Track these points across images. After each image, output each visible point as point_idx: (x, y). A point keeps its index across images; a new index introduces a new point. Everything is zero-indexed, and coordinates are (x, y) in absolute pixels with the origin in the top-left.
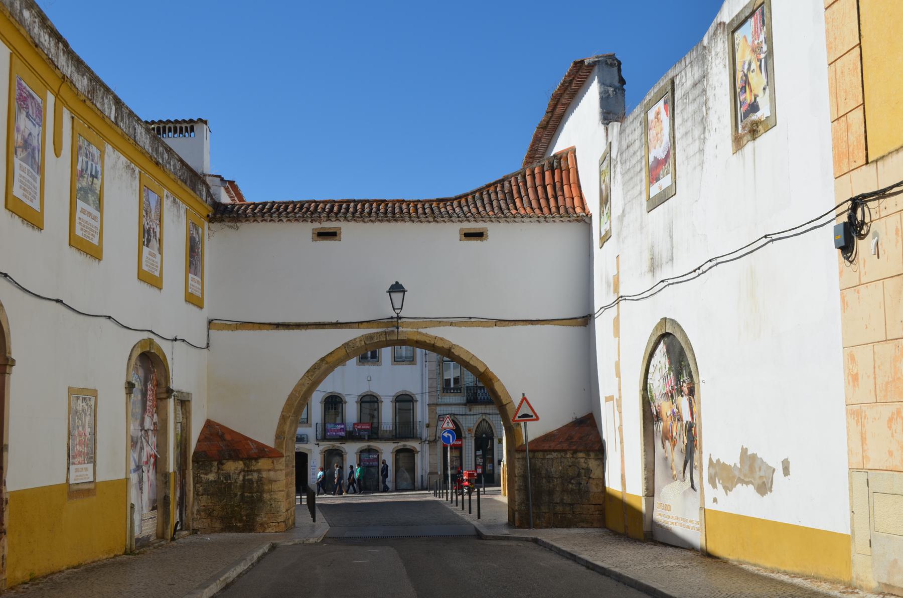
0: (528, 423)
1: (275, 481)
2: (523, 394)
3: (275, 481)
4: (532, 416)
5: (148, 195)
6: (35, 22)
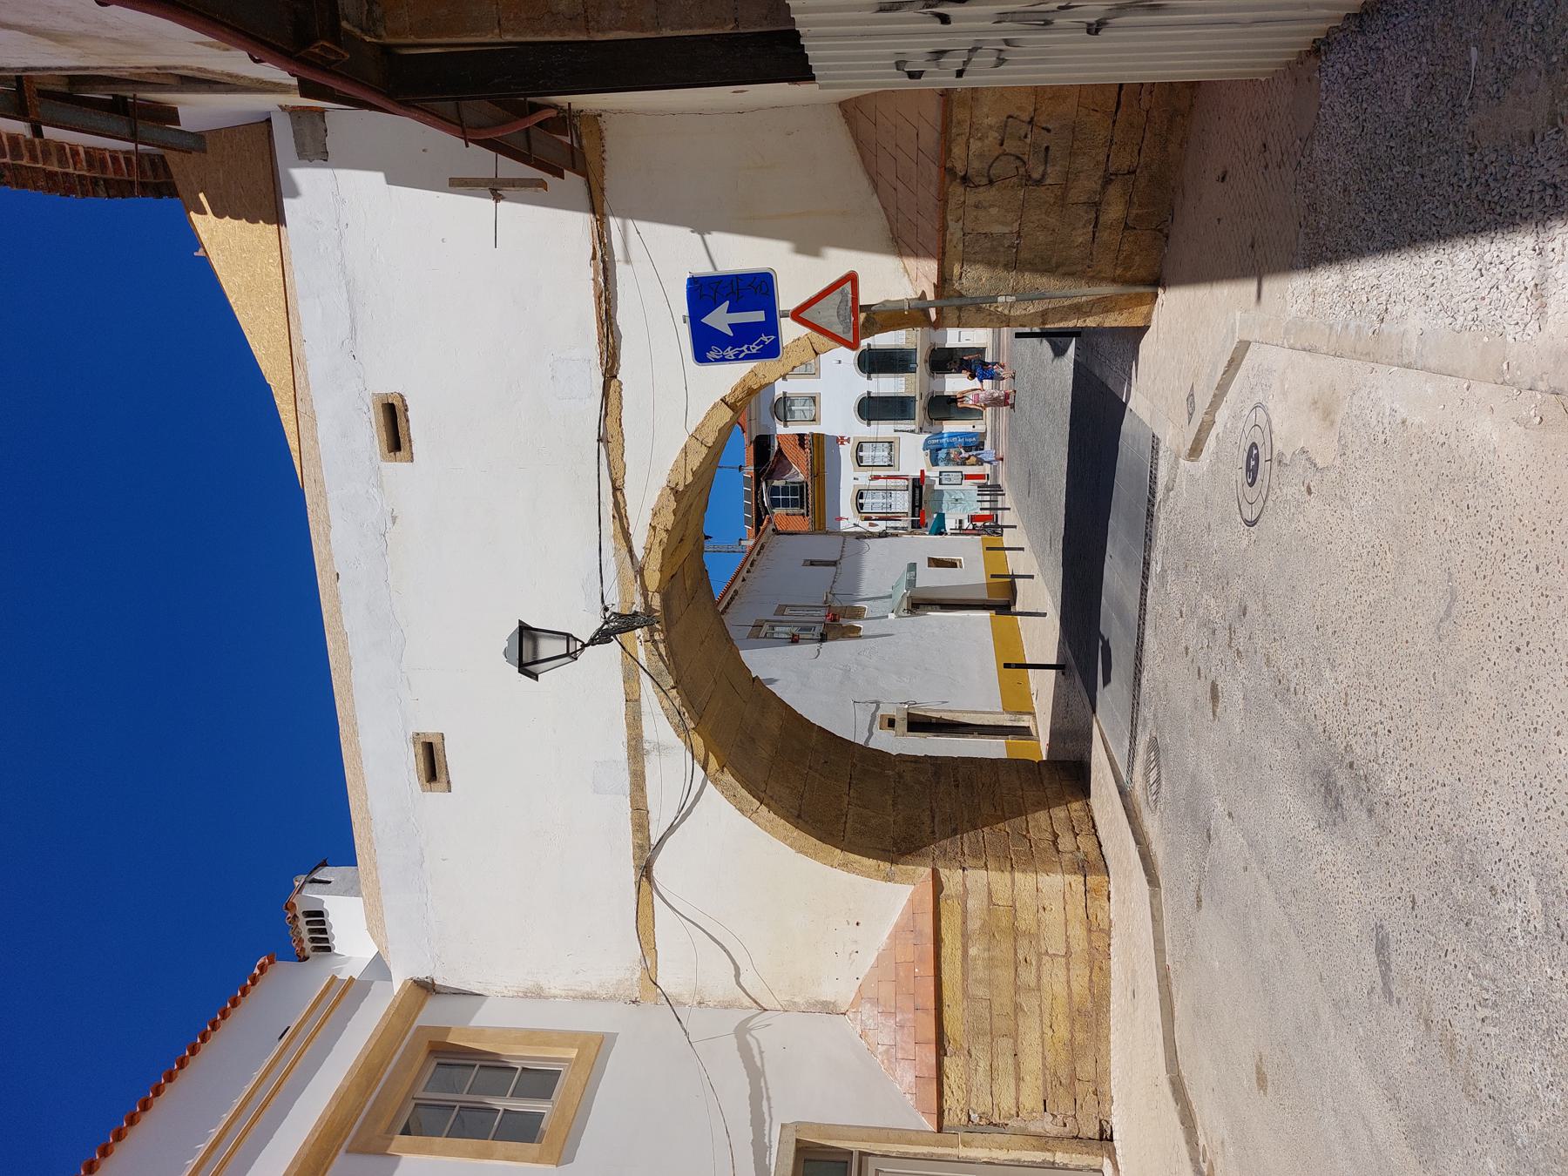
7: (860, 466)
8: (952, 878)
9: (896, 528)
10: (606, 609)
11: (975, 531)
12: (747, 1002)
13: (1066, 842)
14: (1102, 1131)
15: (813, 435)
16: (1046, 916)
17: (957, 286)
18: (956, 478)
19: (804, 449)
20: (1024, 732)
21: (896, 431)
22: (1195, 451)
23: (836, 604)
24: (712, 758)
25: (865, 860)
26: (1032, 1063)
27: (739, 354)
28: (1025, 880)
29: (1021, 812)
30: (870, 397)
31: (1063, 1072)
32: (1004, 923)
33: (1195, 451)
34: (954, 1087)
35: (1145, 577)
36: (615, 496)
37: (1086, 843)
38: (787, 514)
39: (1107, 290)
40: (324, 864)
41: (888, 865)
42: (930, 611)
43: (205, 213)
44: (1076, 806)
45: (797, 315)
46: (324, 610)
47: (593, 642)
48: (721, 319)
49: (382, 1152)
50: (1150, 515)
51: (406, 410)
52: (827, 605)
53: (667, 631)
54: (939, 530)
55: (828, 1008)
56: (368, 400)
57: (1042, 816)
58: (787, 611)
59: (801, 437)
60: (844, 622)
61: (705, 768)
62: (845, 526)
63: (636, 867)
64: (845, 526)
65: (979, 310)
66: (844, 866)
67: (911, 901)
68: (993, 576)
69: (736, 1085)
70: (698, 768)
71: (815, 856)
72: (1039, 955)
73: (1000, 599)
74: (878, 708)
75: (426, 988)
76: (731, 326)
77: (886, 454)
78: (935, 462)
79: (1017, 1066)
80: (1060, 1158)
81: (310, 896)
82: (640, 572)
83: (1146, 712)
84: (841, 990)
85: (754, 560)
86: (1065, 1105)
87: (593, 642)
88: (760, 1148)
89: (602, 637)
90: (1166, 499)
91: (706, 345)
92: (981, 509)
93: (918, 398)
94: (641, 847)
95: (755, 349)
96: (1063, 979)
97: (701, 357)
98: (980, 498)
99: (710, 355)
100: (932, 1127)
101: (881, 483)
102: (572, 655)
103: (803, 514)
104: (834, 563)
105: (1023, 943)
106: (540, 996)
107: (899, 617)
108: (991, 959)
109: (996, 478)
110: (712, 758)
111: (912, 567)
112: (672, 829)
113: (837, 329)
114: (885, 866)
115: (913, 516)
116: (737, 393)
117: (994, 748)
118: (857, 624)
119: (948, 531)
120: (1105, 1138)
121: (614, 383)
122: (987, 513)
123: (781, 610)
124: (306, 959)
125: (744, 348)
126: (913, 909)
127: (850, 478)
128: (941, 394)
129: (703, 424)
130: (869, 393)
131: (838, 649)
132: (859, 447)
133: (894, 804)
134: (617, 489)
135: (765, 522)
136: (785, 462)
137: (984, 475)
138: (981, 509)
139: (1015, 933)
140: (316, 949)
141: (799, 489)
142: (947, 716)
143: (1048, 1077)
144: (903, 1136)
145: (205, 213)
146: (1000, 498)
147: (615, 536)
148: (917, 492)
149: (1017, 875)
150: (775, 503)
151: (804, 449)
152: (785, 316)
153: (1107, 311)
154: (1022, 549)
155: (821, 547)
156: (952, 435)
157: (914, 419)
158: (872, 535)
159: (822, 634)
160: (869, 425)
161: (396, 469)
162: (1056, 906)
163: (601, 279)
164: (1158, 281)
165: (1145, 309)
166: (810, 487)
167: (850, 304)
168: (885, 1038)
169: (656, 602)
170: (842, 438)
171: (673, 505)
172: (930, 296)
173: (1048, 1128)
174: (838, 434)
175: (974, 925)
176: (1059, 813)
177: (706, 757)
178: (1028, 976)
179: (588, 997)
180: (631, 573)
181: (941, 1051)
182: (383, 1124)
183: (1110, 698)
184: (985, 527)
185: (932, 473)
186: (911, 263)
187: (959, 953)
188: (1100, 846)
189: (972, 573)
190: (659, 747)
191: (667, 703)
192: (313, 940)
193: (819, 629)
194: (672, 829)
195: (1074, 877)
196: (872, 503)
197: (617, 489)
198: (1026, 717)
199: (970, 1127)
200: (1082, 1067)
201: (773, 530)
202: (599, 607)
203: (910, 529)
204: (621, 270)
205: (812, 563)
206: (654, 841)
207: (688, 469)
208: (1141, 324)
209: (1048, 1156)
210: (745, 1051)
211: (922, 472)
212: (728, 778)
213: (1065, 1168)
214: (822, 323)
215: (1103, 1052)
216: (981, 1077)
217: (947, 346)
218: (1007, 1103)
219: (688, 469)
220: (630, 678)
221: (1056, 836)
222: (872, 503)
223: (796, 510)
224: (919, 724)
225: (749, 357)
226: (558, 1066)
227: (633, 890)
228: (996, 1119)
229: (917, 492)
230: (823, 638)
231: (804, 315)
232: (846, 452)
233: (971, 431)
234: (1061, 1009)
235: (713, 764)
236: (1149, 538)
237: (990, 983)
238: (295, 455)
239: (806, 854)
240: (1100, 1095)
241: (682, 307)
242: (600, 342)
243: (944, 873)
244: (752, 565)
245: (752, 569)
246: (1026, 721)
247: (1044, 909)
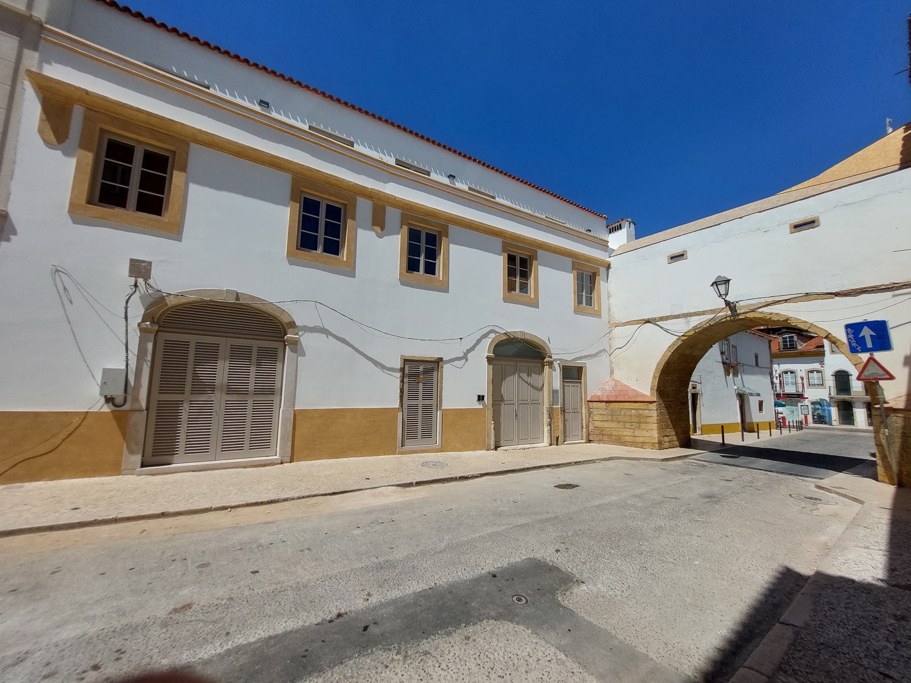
8: (654, 406)
9: (776, 387)
10: (737, 302)
11: (777, 419)
12: (612, 351)
13: (666, 439)
14: (591, 441)
15: (824, 351)
16: (645, 432)
17: (892, 415)
18: (805, 412)
19: (815, 348)
20: (695, 431)
21: (830, 387)
22: (819, 487)
23: (739, 367)
24: (686, 338)
26: (606, 425)
27: (850, 339)
28: (655, 426)
29: (674, 427)
30: (849, 375)
31: (604, 432)
32: (642, 420)
33: (819, 487)
35: (765, 470)
36: (783, 300)
37: (667, 445)
38: (779, 343)
39: (895, 467)
40: (635, 224)
41: (656, 389)
42: (739, 402)
43: (905, 132)
44: (677, 443)
45: (871, 359)
46: (726, 212)
47: (726, 301)
48: (867, 333)
49: (573, 269)
50: (791, 474)
51: (813, 228)
52: (738, 364)
53: (731, 321)
54: (776, 405)
55: (612, 372)
56: (816, 215)
57: (674, 433)
58: (734, 349)
59: (823, 346)
60: (731, 370)
61: (682, 336)
62: (775, 366)
63: (649, 319)
64: (775, 366)
65: (881, 422)
66: (654, 376)
67: (645, 395)
68: (758, 425)
69: (592, 351)
70: (682, 334)
72: (634, 429)
73: (747, 427)
74: (699, 383)
75: (608, 267)
76: (864, 336)
77: (816, 383)
78: (813, 403)
79: (605, 421)
80: (584, 430)
81: (626, 225)
82: (753, 311)
83: (715, 465)
84: (617, 375)
86: (596, 432)
87: (726, 301)
88: (580, 358)
89: (728, 304)
90: (798, 478)
91: (854, 329)
92: (789, 422)
93: (850, 396)
94: (655, 319)
95: (854, 345)
96: (628, 434)
97: (848, 326)
98: (795, 421)
99: (849, 330)
100: (588, 399)
101: (800, 381)
102: (720, 296)
103: (780, 349)
104: (757, 365)
105: (637, 425)
106: (608, 297)
107: (735, 390)
108: (632, 416)
109: (805, 428)
110: (686, 338)
111: (758, 395)
112: (662, 328)
113: (866, 373)
115: (783, 394)
118: (731, 375)
119: (776, 408)
120: (590, 441)
121: (833, 296)
122: (787, 424)
123: (734, 347)
124: (607, 227)
125: (854, 341)
126: (637, 394)
127: (801, 368)
128: (853, 406)
129: (818, 327)
130: (851, 375)
131: (721, 369)
132: (818, 372)
133: (673, 390)
134: (786, 301)
136: (807, 340)
137: (807, 424)
138: (789, 422)
139: (639, 423)
140: (610, 229)
141: (793, 347)
142: (698, 406)
144: (586, 392)
145: (905, 132)
146: (796, 429)
147: (766, 302)
148: (796, 396)
149: (656, 425)
150: (783, 339)
151: (815, 348)
152: (871, 354)
153: (885, 467)
154: (771, 436)
155: (764, 359)
156: (830, 412)
157: (837, 395)
158: (772, 379)
159: (725, 363)
160: (832, 375)
161: (787, 229)
162: (648, 435)
163: (883, 287)
164: (900, 485)
165: (887, 480)
166: (794, 351)
167: (879, 377)
168: (607, 388)
169: (741, 317)
170: (824, 364)
172: (885, 405)
174: (825, 362)
175: (641, 412)
176: (675, 438)
177: (686, 336)
178: (628, 425)
179: (609, 310)
180: (752, 308)
181: (607, 402)
182: (578, 267)
183: (717, 456)
184: (780, 422)
185: (806, 402)
186: (904, 399)
187: (633, 408)
188: (666, 449)
189: (756, 416)
190: (689, 322)
191: (704, 323)
192: (613, 228)
193: (728, 361)
194: (662, 328)
196: (788, 378)
197: (786, 301)
198: (700, 432)
199: (589, 409)
201: (771, 340)
202: (738, 300)
203: (776, 393)
204: (890, 294)
205: (756, 357)
206: (657, 323)
207: (797, 324)
208: (879, 479)
209: (584, 427)
210: (600, 352)
211: (807, 398)
212: (680, 343)
213: (582, 431)
214: (869, 367)
215: (611, 443)
216: (601, 412)
217: (854, 409)
218: (595, 418)
219: (797, 324)
220: (712, 311)
221: (668, 436)
222: (788, 378)
223: (782, 346)
224: (695, 396)
225: (850, 343)
226: (818, 429)
227: (642, 319)
229: (796, 396)
230: (724, 363)
231: (871, 361)
232: (816, 366)
233: (833, 419)
234: (620, 433)
235: (684, 338)
236: (782, 473)
237: (625, 415)
238: (789, 190)
239: (657, 366)
240: (600, 441)
241: (871, 318)
242: (852, 290)
243: (655, 404)
244: (753, 334)
246: (698, 432)
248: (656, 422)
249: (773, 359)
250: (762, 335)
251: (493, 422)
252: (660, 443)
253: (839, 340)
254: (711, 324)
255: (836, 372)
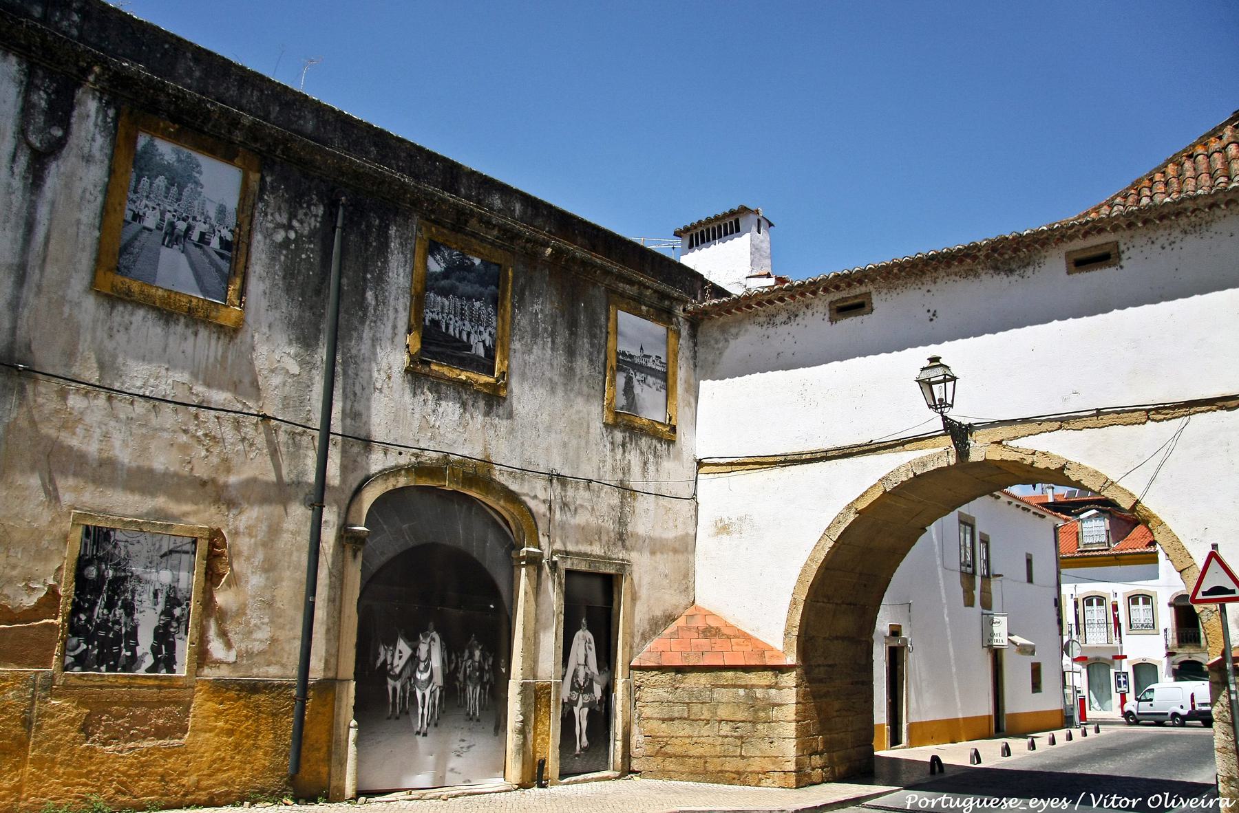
0: (1229, 606)
1: (779, 705)
2: (1215, 546)
3: (779, 705)
4: (1233, 592)
5: (629, 381)
6: (65, 538)
7: (1129, 598)
21: (1166, 630)
25: (798, 617)
31: (668, 749)
34: (656, 677)
41: (797, 633)
66: (794, 602)
71: (800, 581)
85: (1029, 510)
114: (795, 632)
116: (1145, 512)
117: (881, 715)
126: (763, 649)
135: (1065, 517)
143: (665, 739)
171: (1053, 467)
173: (635, 738)
195: (794, 764)
200: (672, 762)
205: (1029, 562)
212: (851, 517)
218: (647, 712)
222: (1095, 614)
224: (896, 657)
228: (638, 704)
231: (1214, 561)
244: (1024, 509)
245: (1020, 509)
247: (771, 743)
248: (794, 717)
249: (1063, 571)
250: (1040, 512)
251: (353, 723)
252: (799, 771)
253: (1154, 517)
254: (918, 473)
255: (1177, 598)
